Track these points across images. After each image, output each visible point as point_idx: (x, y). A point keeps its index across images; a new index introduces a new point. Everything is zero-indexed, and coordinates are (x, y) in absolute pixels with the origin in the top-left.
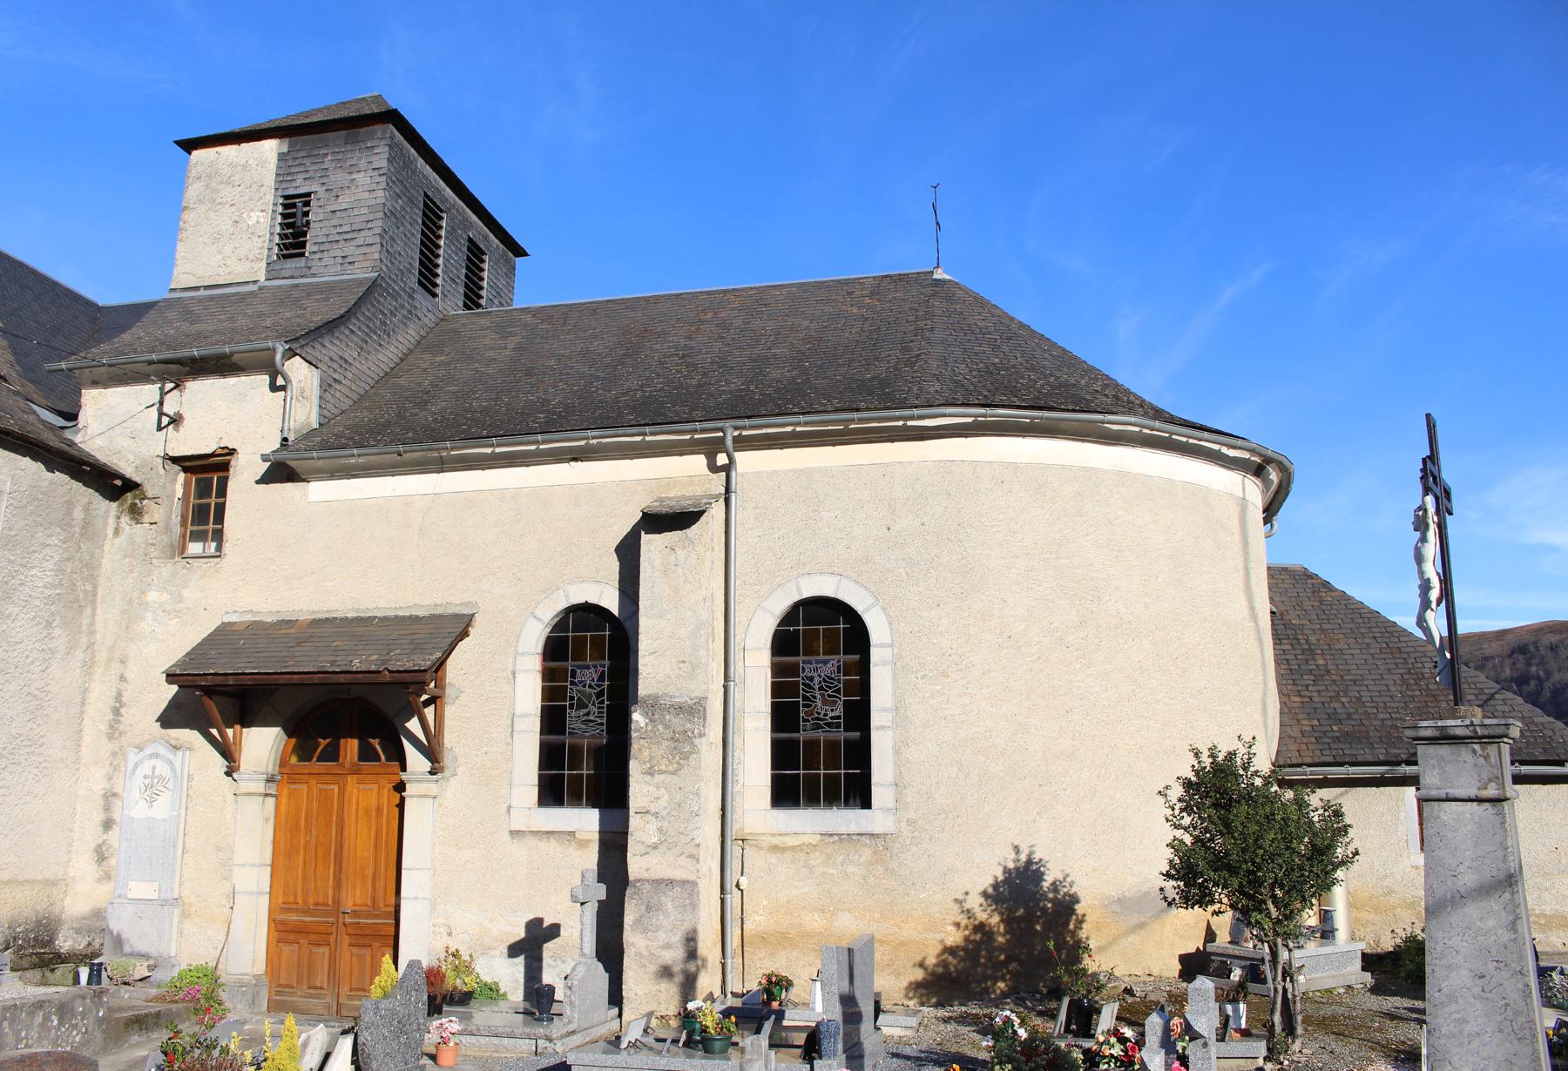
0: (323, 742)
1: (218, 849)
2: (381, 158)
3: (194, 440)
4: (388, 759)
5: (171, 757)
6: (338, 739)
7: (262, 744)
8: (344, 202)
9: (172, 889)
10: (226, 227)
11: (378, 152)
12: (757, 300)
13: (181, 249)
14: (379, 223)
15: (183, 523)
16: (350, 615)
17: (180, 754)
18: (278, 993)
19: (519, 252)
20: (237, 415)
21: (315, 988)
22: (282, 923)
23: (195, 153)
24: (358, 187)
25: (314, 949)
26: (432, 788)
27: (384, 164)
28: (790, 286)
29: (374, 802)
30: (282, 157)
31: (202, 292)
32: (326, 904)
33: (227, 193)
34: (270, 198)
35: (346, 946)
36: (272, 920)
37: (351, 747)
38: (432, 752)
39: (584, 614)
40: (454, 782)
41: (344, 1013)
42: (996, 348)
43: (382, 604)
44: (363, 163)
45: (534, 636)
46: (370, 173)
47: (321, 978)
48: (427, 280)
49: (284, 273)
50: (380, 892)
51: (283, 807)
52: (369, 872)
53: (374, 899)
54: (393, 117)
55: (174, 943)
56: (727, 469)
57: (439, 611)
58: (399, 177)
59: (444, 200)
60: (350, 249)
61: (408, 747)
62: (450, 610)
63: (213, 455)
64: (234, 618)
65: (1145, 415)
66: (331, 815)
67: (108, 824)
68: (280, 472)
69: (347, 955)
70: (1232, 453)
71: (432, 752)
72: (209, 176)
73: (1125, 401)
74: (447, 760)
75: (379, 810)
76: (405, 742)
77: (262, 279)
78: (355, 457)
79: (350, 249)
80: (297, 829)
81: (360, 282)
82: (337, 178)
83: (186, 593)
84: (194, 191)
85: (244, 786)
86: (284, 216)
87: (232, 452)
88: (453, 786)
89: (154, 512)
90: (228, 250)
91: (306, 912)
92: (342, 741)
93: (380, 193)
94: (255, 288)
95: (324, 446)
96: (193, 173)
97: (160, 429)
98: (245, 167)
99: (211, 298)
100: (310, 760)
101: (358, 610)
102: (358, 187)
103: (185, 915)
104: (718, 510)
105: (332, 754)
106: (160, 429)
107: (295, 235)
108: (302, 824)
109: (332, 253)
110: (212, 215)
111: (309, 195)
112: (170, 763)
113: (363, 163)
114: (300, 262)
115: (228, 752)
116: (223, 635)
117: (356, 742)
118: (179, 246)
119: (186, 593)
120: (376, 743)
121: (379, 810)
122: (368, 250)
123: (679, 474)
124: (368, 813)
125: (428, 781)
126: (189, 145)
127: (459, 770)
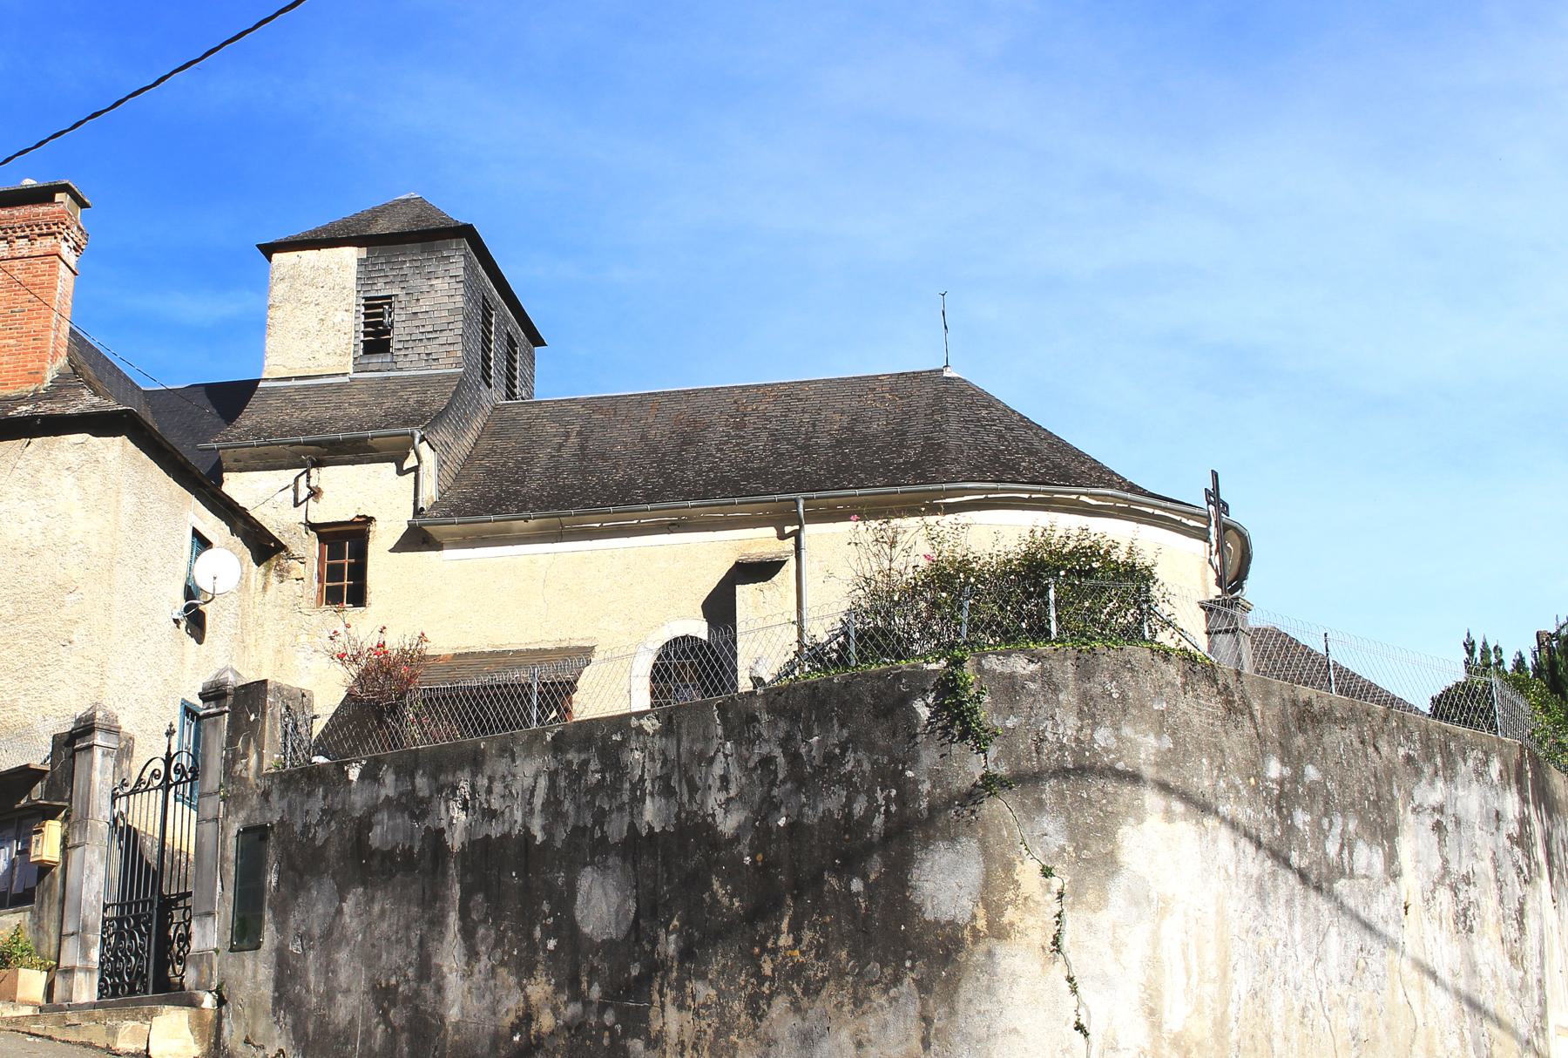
2: (457, 266)
3: (323, 512)
8: (425, 304)
10: (313, 324)
11: (457, 261)
12: (789, 394)
13: (270, 343)
14: (460, 325)
15: (320, 581)
16: (487, 650)
19: (537, 340)
20: (372, 493)
23: (276, 257)
24: (437, 294)
27: (461, 272)
28: (816, 382)
30: (361, 262)
31: (293, 383)
33: (311, 293)
34: (353, 298)
39: (680, 647)
42: (1001, 437)
44: (440, 272)
45: (644, 664)
46: (447, 279)
48: (486, 377)
49: (371, 367)
54: (467, 233)
56: (797, 535)
57: (564, 645)
58: (470, 284)
59: (493, 299)
60: (433, 347)
62: (574, 644)
63: (351, 522)
65: (1121, 489)
68: (417, 539)
70: (1192, 523)
72: (292, 277)
73: (1102, 475)
77: (351, 370)
78: (491, 522)
79: (433, 347)
81: (449, 377)
82: (416, 282)
84: (278, 290)
86: (367, 316)
87: (370, 520)
89: (297, 568)
90: (316, 346)
93: (459, 298)
94: (346, 379)
95: (458, 511)
96: (276, 275)
97: (296, 504)
98: (327, 270)
99: (307, 388)
102: (437, 294)
104: (792, 561)
106: (296, 504)
107: (377, 334)
109: (416, 350)
110: (298, 313)
111: (389, 297)
113: (440, 272)
114: (388, 358)
118: (269, 341)
122: (451, 348)
123: (761, 541)
126: (268, 250)
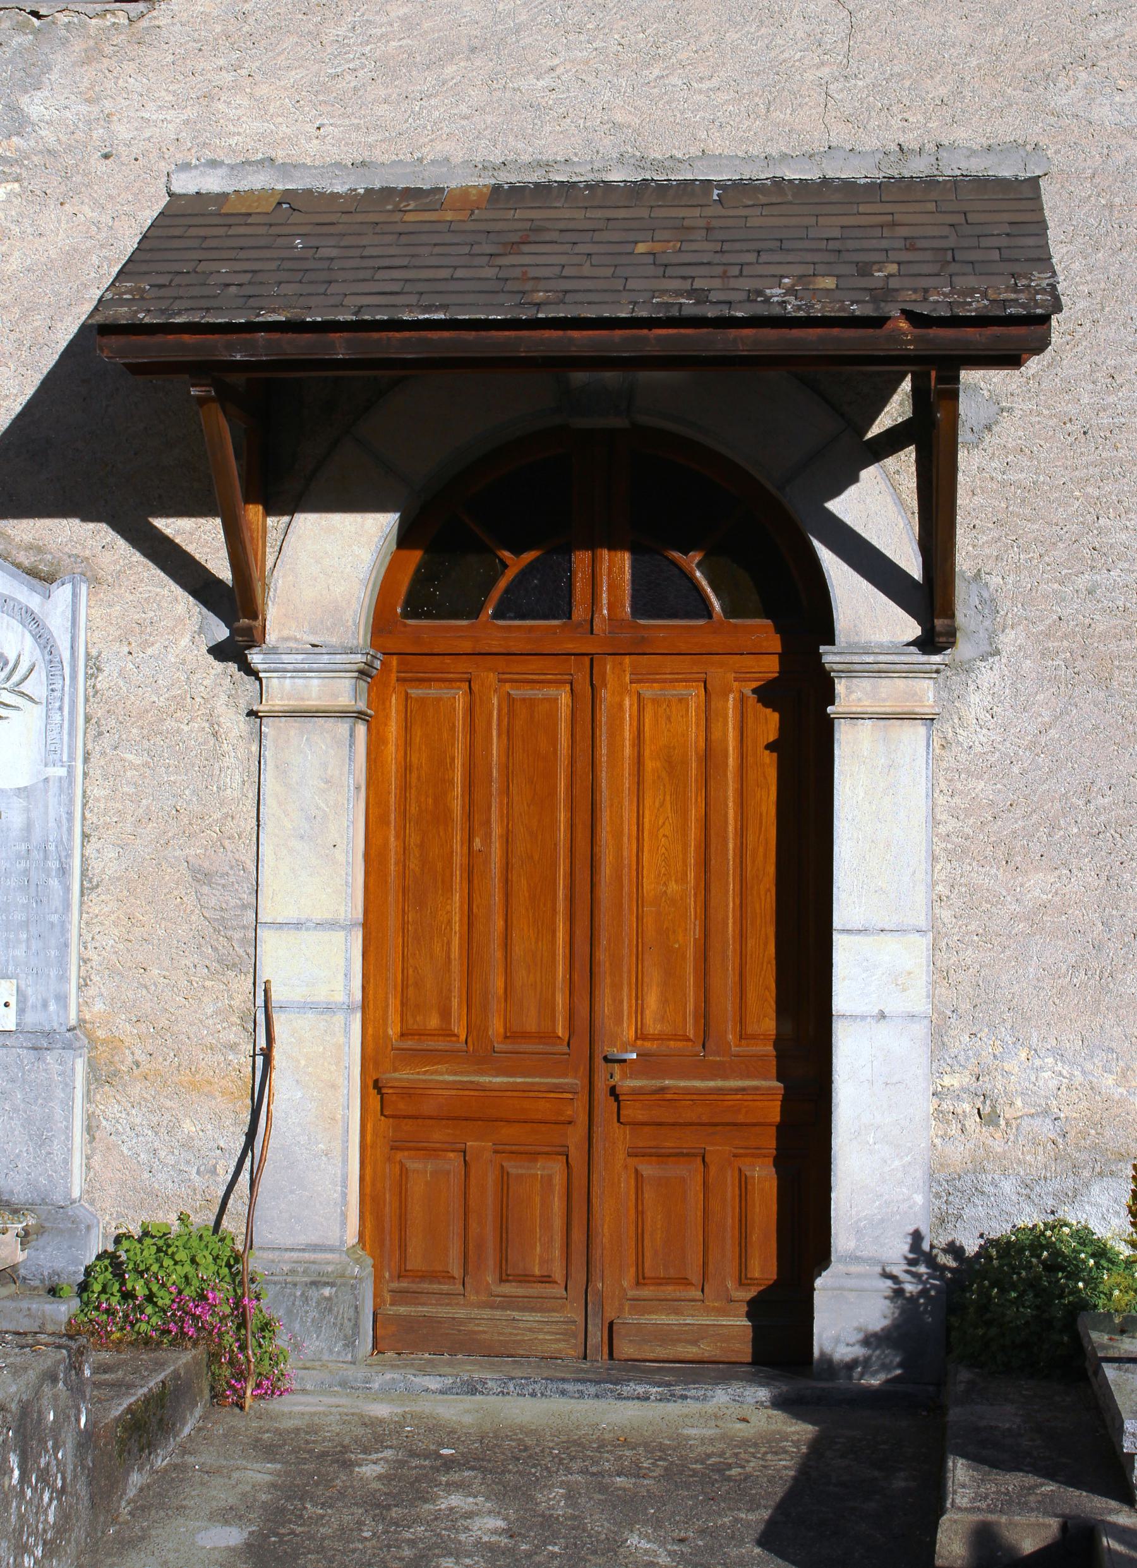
0: (516, 563)
1: (202, 876)
4: (731, 611)
5: (33, 601)
6: (567, 550)
7: (331, 563)
9: (62, 999)
17: (62, 593)
18: (400, 1296)
21: (525, 1279)
22: (408, 1092)
25: (514, 1168)
26: (924, 693)
29: (694, 734)
32: (548, 1037)
35: (621, 1155)
36: (375, 1087)
37: (609, 576)
38: (931, 601)
40: (988, 675)
41: (625, 1349)
43: (718, 144)
47: (545, 1252)
50: (726, 1004)
51: (391, 751)
52: (688, 939)
53: (705, 1017)
55: (77, 1161)
61: (842, 580)
64: (213, 183)
66: (550, 775)
67: (882, 1016)
69: (626, 1185)
71: (931, 601)
74: (965, 613)
75: (710, 757)
76: (827, 557)
80: (440, 816)
83: (35, 106)
85: (281, 690)
88: (990, 688)
91: (482, 1056)
92: (581, 559)
100: (474, 612)
101: (641, 162)
103: (102, 1076)
105: (547, 596)
108: (457, 806)
112: (33, 622)
115: (235, 607)
116: (185, 230)
117: (625, 560)
119: (35, 106)
120: (692, 562)
121: (710, 757)
124: (673, 766)
125: (911, 672)
127: (1008, 640)
